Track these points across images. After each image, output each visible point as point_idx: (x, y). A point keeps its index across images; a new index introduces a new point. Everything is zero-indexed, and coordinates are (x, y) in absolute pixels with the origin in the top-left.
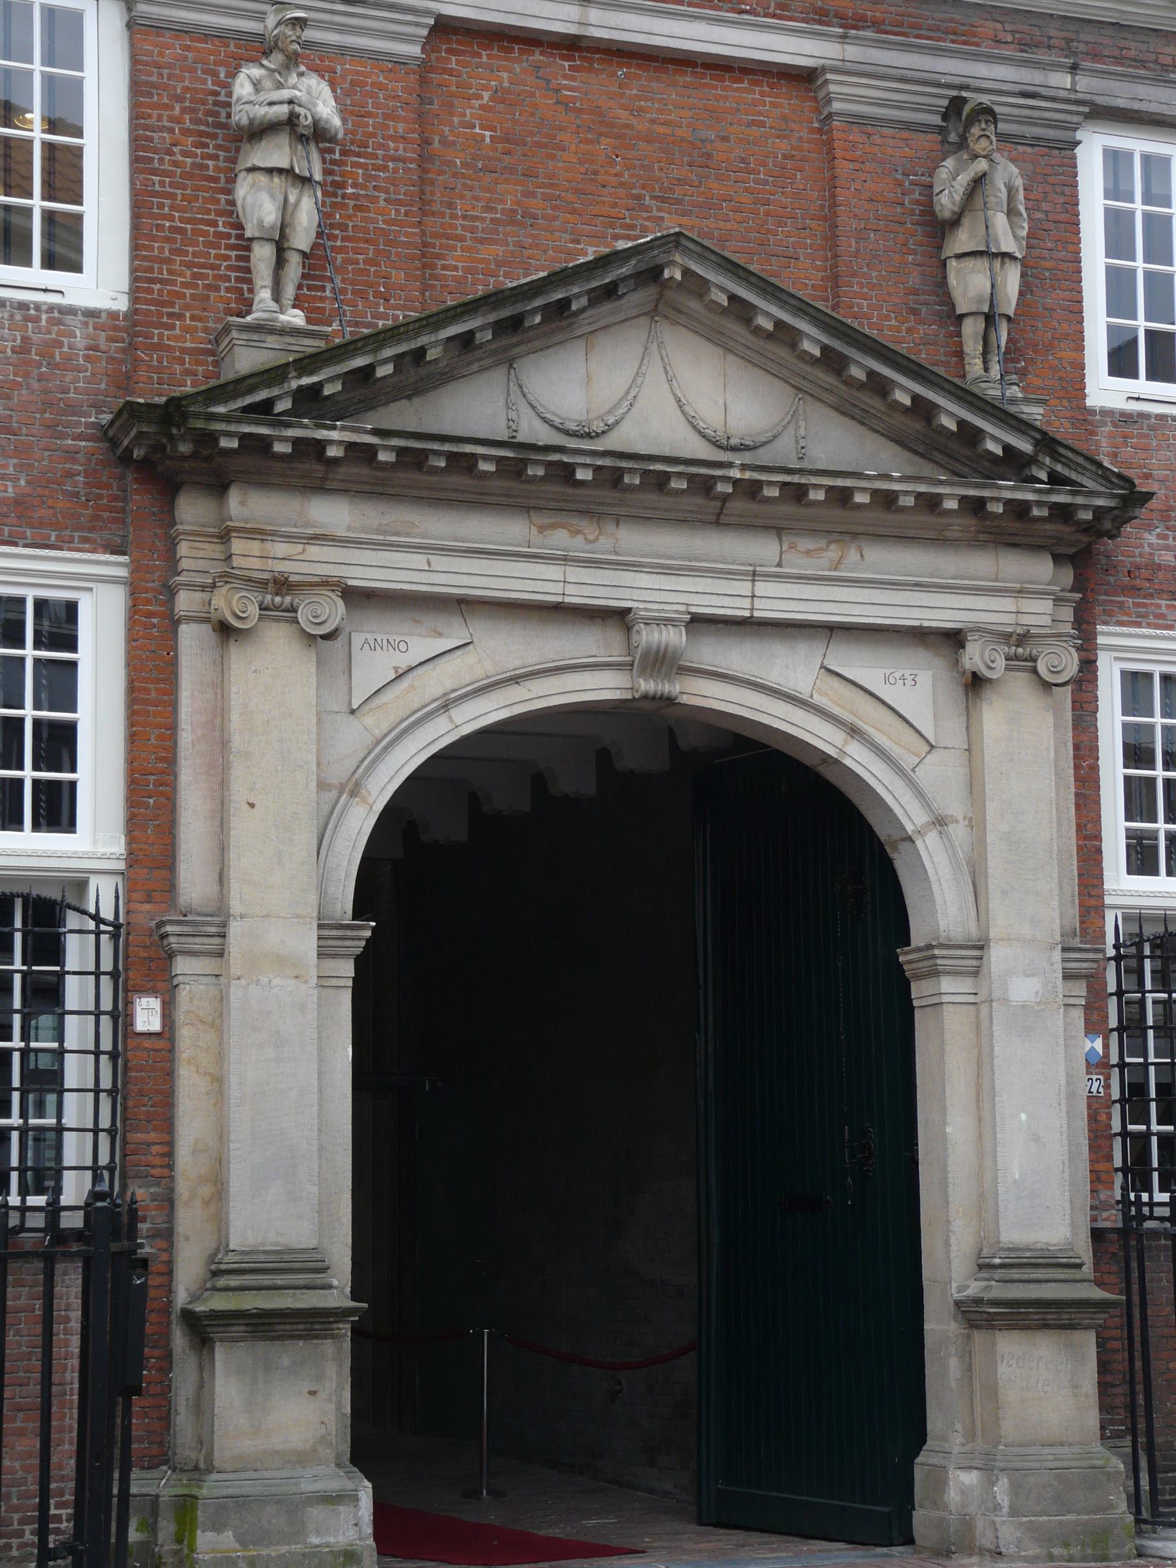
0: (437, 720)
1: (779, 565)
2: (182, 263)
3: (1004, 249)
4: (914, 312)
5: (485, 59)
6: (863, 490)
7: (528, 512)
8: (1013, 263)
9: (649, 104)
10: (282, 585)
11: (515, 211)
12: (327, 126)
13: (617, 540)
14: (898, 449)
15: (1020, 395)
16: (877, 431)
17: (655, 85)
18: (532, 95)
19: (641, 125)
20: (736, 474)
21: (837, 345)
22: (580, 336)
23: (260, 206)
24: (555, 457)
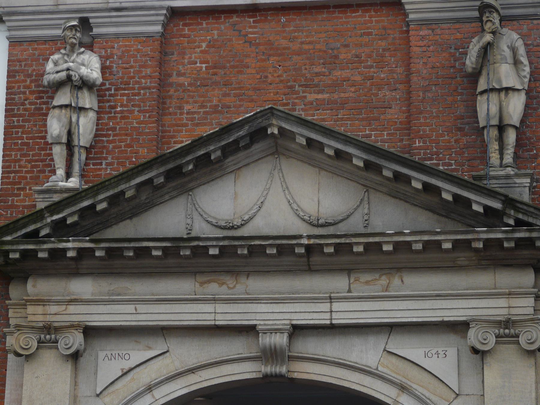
0: (145, 397)
1: (349, 291)
2: (27, 161)
3: (505, 85)
4: (460, 129)
5: (204, 25)
6: (388, 243)
7: (195, 275)
8: (516, 94)
9: (300, 34)
10: (48, 328)
11: (218, 106)
12: (88, 79)
13: (247, 286)
14: (430, 214)
15: (512, 173)
16: (417, 206)
17: (304, 23)
18: (230, 40)
19: (295, 46)
20: (305, 241)
21: (372, 158)
22: (231, 172)
24: (195, 243)
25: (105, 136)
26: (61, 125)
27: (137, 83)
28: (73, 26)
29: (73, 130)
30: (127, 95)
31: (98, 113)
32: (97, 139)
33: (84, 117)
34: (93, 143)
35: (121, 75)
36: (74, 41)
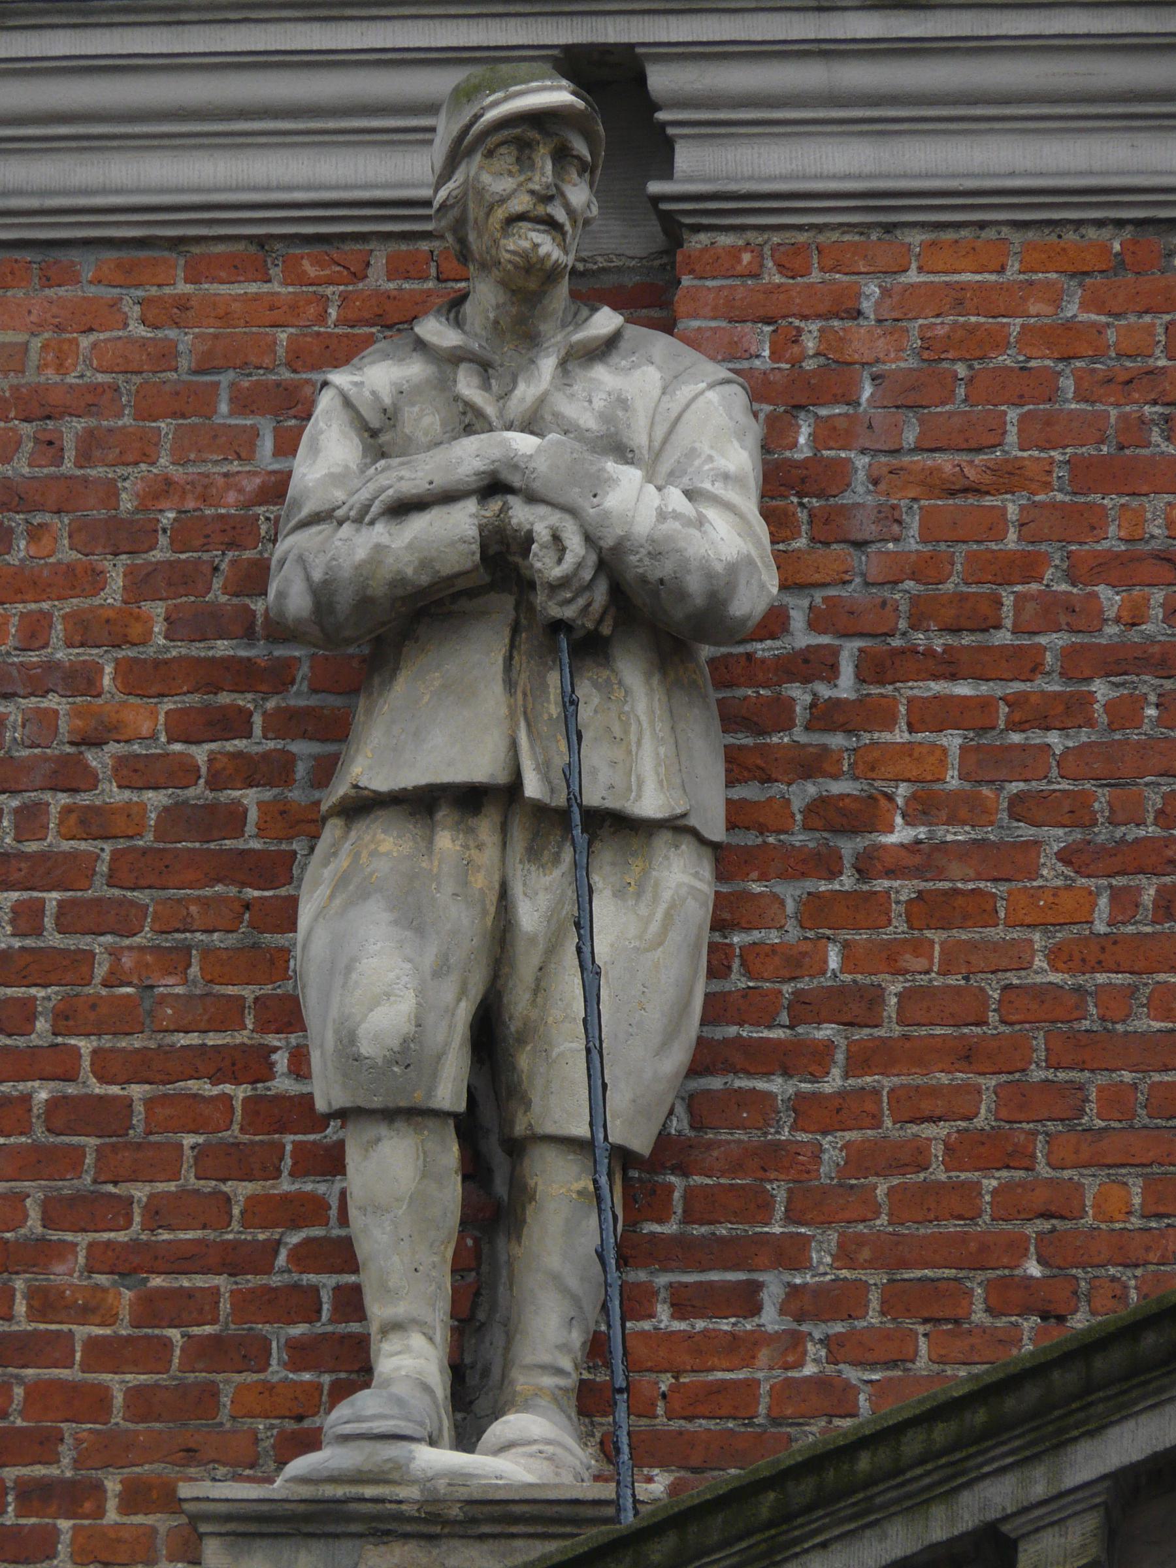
2: (105, 1259)
12: (666, 569)
23: (349, 969)
25: (783, 1059)
26: (429, 959)
27: (1053, 613)
28: (541, 120)
29: (519, 1003)
30: (971, 716)
31: (726, 861)
32: (715, 1083)
33: (619, 893)
34: (679, 1124)
35: (912, 544)
36: (547, 246)
